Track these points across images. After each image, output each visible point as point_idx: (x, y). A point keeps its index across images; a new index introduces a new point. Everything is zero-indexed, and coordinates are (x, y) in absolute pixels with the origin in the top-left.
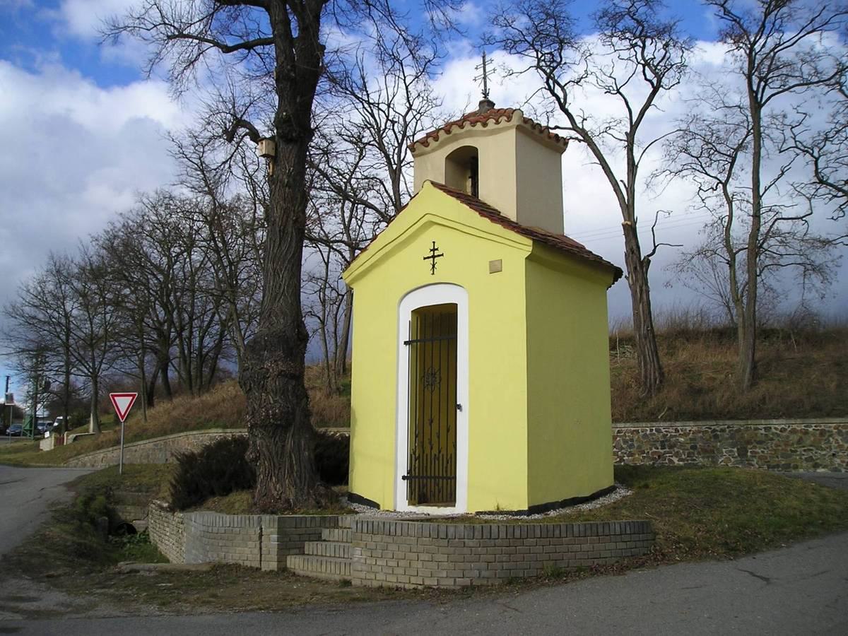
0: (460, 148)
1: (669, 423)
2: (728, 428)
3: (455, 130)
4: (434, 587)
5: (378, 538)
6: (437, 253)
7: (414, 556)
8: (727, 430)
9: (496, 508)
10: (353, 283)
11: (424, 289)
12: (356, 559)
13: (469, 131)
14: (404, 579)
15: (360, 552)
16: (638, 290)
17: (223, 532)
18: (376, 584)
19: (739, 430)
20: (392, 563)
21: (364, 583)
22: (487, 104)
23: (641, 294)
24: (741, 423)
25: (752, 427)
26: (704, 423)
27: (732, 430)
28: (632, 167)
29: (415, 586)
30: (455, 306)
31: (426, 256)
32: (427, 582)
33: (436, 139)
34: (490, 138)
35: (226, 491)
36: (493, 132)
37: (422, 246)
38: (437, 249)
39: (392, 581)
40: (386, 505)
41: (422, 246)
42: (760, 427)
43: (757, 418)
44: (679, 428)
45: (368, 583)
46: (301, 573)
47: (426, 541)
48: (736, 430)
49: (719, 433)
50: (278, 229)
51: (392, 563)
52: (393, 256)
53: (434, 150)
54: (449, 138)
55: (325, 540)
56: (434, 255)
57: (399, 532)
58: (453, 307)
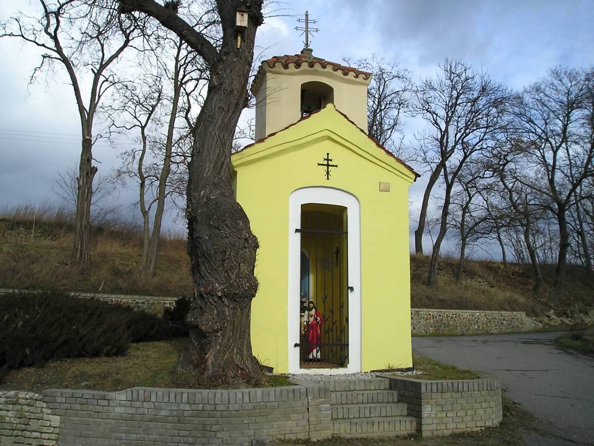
1: (107, 295)
2: (147, 301)
3: (318, 67)
5: (447, 395)
7: (477, 405)
8: (146, 303)
9: (388, 367)
11: (343, 193)
12: (426, 415)
13: (330, 73)
14: (470, 424)
15: (430, 409)
16: (86, 190)
17: (253, 408)
18: (447, 433)
19: (153, 304)
20: (461, 414)
21: (435, 433)
22: (307, 51)
23: (88, 194)
24: (156, 298)
25: (162, 301)
26: (131, 297)
27: (149, 303)
30: (303, 207)
33: (298, 65)
36: (349, 82)
37: (319, 152)
38: (331, 160)
39: (462, 427)
41: (319, 152)
42: (166, 302)
43: (165, 296)
44: (113, 299)
45: (440, 433)
48: (152, 303)
49: (140, 305)
51: (461, 414)
56: (328, 164)
57: (466, 388)
58: (343, 209)
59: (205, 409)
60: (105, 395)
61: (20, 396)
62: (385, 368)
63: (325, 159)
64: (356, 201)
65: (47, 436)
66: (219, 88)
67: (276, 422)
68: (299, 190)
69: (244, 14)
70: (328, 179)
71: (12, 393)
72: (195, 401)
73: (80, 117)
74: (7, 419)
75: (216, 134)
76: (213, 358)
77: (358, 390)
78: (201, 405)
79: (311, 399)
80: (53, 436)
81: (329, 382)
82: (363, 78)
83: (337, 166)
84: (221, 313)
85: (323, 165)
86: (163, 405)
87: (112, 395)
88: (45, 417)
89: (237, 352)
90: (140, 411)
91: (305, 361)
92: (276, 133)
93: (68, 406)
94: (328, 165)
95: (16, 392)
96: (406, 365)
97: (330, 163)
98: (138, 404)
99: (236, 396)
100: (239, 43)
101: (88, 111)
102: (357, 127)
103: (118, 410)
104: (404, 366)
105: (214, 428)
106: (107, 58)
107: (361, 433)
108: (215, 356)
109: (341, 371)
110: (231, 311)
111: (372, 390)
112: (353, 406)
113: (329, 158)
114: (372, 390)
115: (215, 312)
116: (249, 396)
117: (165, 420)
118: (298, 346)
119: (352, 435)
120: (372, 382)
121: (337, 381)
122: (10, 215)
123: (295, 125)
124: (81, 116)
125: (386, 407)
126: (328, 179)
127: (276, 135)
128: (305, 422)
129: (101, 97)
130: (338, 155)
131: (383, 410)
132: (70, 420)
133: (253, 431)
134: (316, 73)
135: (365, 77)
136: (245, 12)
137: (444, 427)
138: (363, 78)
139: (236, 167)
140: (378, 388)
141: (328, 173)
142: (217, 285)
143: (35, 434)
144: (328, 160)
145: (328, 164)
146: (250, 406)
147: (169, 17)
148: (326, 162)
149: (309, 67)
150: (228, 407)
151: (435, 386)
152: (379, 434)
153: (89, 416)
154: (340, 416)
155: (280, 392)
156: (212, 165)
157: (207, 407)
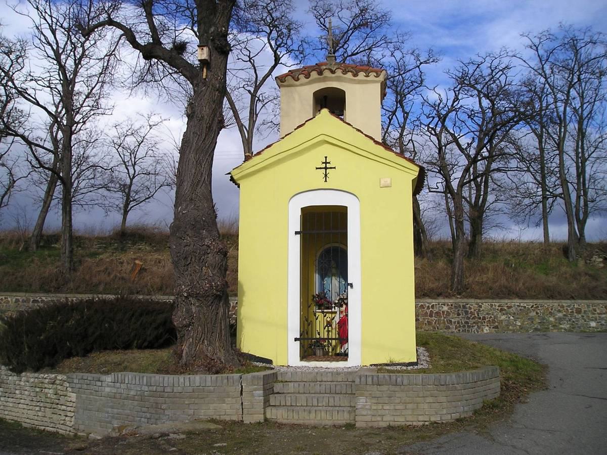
0: (322, 89)
4: (439, 422)
5: (385, 388)
6: (328, 166)
10: (240, 180)
17: (191, 391)
26: (531, 301)
28: (253, 114)
29: (423, 423)
31: (317, 167)
32: (433, 419)
34: (357, 86)
35: (86, 352)
37: (316, 157)
38: (329, 163)
39: (400, 421)
40: (277, 362)
41: (316, 157)
45: (375, 425)
46: (285, 421)
47: (430, 387)
50: (205, 126)
52: (284, 162)
53: (302, 85)
54: (320, 78)
55: (278, 393)
58: (345, 209)
59: (158, 390)
60: (83, 376)
61: (58, 378)
62: (386, 362)
63: (323, 163)
64: (355, 197)
65: (69, 409)
66: (192, 116)
67: (212, 404)
68: (297, 196)
69: (203, 48)
70: (326, 181)
71: (53, 375)
72: (151, 384)
73: (241, 136)
74: (49, 395)
75: (191, 156)
76: (187, 349)
77: (325, 381)
78: (155, 387)
79: (245, 386)
80: (72, 409)
81: (296, 373)
82: (375, 76)
83: (335, 168)
84: (188, 311)
85: (320, 168)
86: (132, 386)
87: (103, 377)
88: (69, 394)
89: (207, 344)
90: (119, 391)
91: (304, 356)
92: (272, 145)
93: (79, 385)
94: (326, 168)
95: (56, 375)
96: (410, 359)
97: (328, 166)
98: (118, 384)
99: (179, 380)
100: (205, 74)
101: (248, 129)
102: (353, 128)
103: (108, 389)
104: (407, 360)
105: (164, 406)
106: (260, 78)
107: (298, 420)
108: (189, 348)
109: (340, 364)
110: (197, 309)
111: (340, 382)
112: (300, 395)
113: (327, 161)
114: (340, 382)
115: (184, 310)
116: (190, 381)
117: (133, 399)
118: (298, 340)
119: (289, 421)
120: (340, 374)
121: (337, 373)
122: (105, 234)
123: (290, 135)
124: (241, 134)
125: (334, 397)
126: (326, 181)
127: (272, 147)
128: (239, 406)
129: (258, 115)
130: (336, 157)
131: (331, 400)
132: (81, 396)
133: (193, 411)
134: (326, 79)
135: (375, 75)
136: (204, 46)
137: (379, 419)
138: (375, 76)
139: (238, 180)
140: (346, 380)
141: (326, 175)
142: (183, 287)
143: (64, 407)
144: (326, 163)
145: (326, 166)
146: (190, 389)
147: (170, 58)
148: (324, 166)
149: (319, 75)
150: (173, 390)
151: (371, 378)
152: (316, 422)
153: (91, 394)
154: (288, 404)
155: (215, 379)
156: (189, 184)
157: (159, 389)
